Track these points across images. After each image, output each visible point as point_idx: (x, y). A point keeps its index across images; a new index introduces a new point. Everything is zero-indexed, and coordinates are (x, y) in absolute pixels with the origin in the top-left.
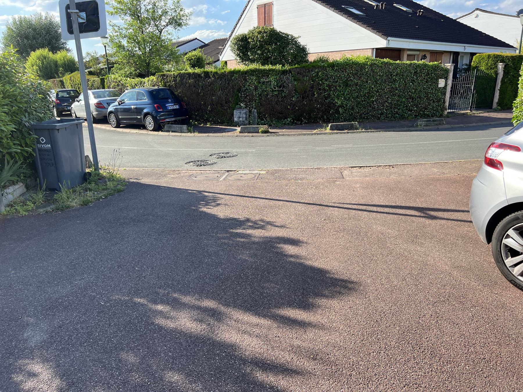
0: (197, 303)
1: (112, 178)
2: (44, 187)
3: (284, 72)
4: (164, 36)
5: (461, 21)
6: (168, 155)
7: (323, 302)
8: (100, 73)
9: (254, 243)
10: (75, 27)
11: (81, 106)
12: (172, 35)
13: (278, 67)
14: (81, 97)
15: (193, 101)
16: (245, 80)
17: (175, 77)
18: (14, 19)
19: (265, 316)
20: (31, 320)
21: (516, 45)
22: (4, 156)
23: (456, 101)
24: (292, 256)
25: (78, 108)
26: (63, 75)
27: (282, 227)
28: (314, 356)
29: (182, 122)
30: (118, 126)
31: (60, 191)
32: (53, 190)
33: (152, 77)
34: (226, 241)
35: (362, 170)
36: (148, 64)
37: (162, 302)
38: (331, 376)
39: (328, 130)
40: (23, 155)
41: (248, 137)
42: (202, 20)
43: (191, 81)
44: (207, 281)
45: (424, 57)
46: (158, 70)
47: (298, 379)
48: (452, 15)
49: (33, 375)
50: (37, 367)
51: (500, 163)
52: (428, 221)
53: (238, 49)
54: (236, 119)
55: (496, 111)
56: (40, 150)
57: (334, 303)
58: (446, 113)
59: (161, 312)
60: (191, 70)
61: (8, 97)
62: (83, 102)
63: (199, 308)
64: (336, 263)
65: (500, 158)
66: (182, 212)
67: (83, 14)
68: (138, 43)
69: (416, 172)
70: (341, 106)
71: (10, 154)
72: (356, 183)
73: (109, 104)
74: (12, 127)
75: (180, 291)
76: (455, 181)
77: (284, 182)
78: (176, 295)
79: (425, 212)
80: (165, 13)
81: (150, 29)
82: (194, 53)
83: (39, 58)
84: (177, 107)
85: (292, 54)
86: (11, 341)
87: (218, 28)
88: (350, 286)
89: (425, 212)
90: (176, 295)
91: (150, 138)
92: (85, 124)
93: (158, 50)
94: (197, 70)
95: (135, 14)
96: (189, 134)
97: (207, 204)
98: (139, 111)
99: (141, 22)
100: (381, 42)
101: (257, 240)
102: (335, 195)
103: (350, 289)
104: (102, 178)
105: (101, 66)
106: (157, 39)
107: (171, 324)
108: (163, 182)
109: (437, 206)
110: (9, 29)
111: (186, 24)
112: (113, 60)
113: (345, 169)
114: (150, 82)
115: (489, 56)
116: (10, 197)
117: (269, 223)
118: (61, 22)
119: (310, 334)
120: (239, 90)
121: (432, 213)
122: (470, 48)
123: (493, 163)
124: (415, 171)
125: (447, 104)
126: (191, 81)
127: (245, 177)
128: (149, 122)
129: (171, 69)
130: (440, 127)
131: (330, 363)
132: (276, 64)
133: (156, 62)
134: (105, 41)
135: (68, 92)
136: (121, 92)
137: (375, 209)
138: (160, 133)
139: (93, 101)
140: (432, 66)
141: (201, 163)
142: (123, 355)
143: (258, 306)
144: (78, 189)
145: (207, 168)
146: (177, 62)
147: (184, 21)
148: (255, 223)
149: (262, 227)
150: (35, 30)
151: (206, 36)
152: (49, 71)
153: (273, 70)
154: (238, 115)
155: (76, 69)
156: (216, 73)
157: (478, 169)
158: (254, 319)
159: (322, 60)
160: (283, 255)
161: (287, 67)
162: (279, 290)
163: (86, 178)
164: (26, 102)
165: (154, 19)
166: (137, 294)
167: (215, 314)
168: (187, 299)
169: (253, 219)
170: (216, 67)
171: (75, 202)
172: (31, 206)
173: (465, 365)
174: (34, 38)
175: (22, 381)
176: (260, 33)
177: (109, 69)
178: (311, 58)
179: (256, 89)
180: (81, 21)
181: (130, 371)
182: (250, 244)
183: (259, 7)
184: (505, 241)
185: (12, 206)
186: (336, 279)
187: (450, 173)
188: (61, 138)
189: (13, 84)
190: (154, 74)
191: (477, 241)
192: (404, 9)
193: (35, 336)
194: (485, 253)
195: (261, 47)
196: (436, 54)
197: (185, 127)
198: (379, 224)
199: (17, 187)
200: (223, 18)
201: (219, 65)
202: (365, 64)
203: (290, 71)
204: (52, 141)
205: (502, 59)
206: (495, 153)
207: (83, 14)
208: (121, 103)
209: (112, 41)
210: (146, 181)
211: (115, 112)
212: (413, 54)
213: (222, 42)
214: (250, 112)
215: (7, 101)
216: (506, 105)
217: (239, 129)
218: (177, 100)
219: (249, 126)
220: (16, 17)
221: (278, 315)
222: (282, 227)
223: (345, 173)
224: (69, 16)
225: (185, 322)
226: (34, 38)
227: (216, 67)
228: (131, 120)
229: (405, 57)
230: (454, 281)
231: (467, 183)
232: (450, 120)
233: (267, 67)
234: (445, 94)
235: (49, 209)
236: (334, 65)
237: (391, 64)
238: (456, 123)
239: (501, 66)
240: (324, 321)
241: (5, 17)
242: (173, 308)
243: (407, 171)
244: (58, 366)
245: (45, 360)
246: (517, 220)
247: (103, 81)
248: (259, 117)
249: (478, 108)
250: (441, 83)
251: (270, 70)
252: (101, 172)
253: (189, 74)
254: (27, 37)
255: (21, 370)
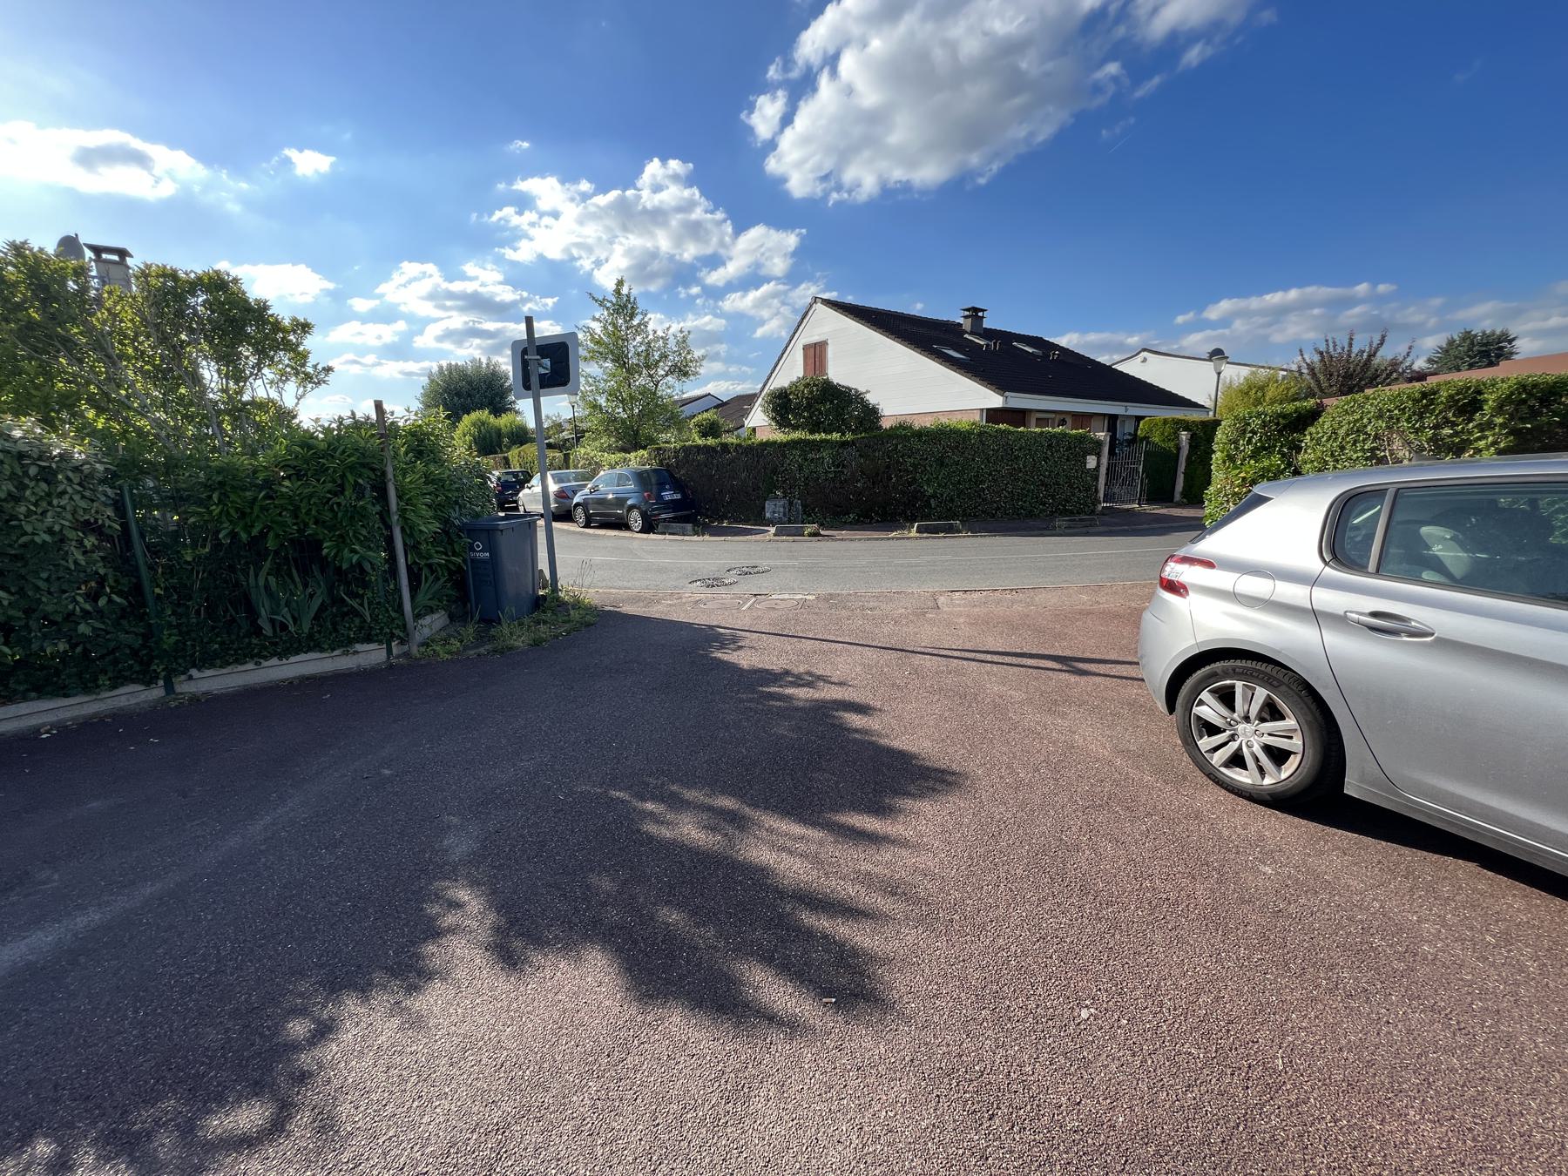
0: (708, 801)
1: (577, 604)
2: (477, 617)
3: (844, 444)
4: (663, 390)
5: (1119, 367)
6: (661, 570)
7: (908, 803)
8: (561, 445)
9: (797, 709)
10: (535, 380)
11: (533, 495)
12: (674, 389)
13: (835, 436)
14: (536, 481)
15: (703, 486)
16: (784, 456)
17: (676, 451)
18: (441, 368)
19: (814, 825)
20: (455, 820)
21: (1208, 404)
22: (420, 569)
23: (1116, 490)
24: (857, 731)
25: (530, 498)
26: (509, 449)
27: (841, 684)
28: (892, 889)
29: (685, 520)
30: (587, 526)
31: (499, 623)
32: (489, 621)
33: (641, 452)
34: (753, 705)
35: (967, 596)
36: (636, 433)
37: (654, 798)
38: (920, 920)
39: (914, 533)
40: (448, 569)
41: (787, 543)
42: (717, 366)
43: (701, 457)
44: (723, 766)
45: (1063, 423)
46: (652, 441)
47: (868, 925)
48: (1104, 359)
49: (457, 905)
50: (463, 895)
51: (1184, 587)
52: (1073, 679)
53: (774, 410)
54: (768, 515)
55: (1179, 505)
56: (472, 561)
57: (925, 806)
58: (1099, 508)
59: (651, 813)
60: (700, 442)
61: (433, 482)
62: (538, 489)
63: (710, 809)
64: (927, 744)
65: (1184, 579)
66: (683, 658)
67: (547, 362)
68: (622, 401)
69: (1054, 601)
70: (934, 496)
71: (430, 566)
72: (1268, 856)
73: (575, 493)
74: (436, 526)
75: (680, 781)
76: (1117, 616)
77: (844, 613)
78: (674, 788)
79: (1069, 663)
80: (664, 356)
81: (641, 381)
82: (705, 415)
83: (474, 424)
84: (678, 496)
85: (857, 417)
86: (424, 851)
87: (742, 378)
88: (950, 779)
89: (1069, 663)
90: (674, 788)
91: (635, 544)
92: (541, 522)
93: (651, 412)
94: (710, 441)
95: (620, 359)
96: (695, 538)
97: (722, 646)
98: (620, 502)
99: (628, 371)
100: (995, 400)
101: (801, 704)
102: (927, 635)
103: (950, 784)
104: (562, 604)
105: (565, 435)
106: (650, 395)
107: (666, 833)
108: (656, 611)
109: (1088, 655)
110: (432, 381)
111: (695, 374)
112: (584, 426)
113: (942, 593)
114: (638, 460)
115: (1165, 422)
116: (426, 631)
117: (820, 678)
118: (328, 278)
119: (887, 854)
120: (774, 471)
121: (1081, 665)
122: (1135, 410)
123: (1174, 587)
124: (1052, 599)
125: (1101, 495)
126: (701, 457)
127: (782, 605)
128: (636, 519)
129: (670, 439)
130: (1092, 530)
131: (917, 901)
132: (831, 432)
133: (647, 430)
134: (573, 398)
135: (515, 475)
136: (594, 473)
137: (989, 657)
138: (652, 536)
139: (553, 487)
140: (1075, 436)
141: (714, 582)
142: (593, 879)
143: (804, 808)
144: (526, 621)
145: (722, 590)
146: (680, 430)
147: (692, 367)
148: (798, 677)
149: (810, 685)
150: (470, 383)
151: (724, 389)
152: (488, 443)
153: (827, 441)
154: (771, 508)
155: (532, 440)
156: (739, 445)
157: (1150, 597)
158: (798, 829)
159: (902, 427)
160: (844, 729)
161: (849, 437)
162: (837, 783)
163: (538, 603)
164: (457, 490)
165: (648, 367)
166: (614, 784)
167: (733, 818)
168: (690, 795)
169: (796, 671)
170: (738, 437)
171: (520, 641)
172: (456, 644)
173: (1137, 908)
174: (469, 395)
175: (438, 914)
176: (807, 385)
177: (578, 439)
178: (886, 424)
179: (800, 468)
180: (542, 371)
181: (604, 904)
182: (791, 710)
183: (806, 348)
184: (1197, 710)
185: (427, 645)
186: (928, 768)
187: (1108, 602)
188: (504, 542)
189: (438, 462)
190: (644, 448)
191: (1153, 709)
192: (1030, 350)
193: (459, 845)
194: (1166, 729)
195: (809, 407)
196: (1082, 419)
197: (689, 526)
198: (995, 682)
199: (436, 616)
200: (750, 364)
201: (744, 433)
202: (970, 433)
203: (853, 443)
204: (491, 547)
205: (1187, 426)
206: (1174, 571)
207: (547, 362)
208: (595, 490)
209: (583, 398)
210: (628, 609)
211: (584, 505)
212: (1044, 418)
213: (749, 399)
214: (791, 503)
215: (431, 488)
216: (1194, 497)
217: (773, 530)
218: (678, 486)
219: (789, 526)
220: (444, 364)
221: (835, 824)
222: (841, 684)
223: (942, 600)
224: (525, 364)
225: (690, 831)
226: (469, 395)
227: (738, 437)
228: (607, 518)
229: (1033, 421)
230: (1117, 775)
231: (1134, 618)
232: (1106, 518)
233: (817, 437)
234: (1097, 479)
235: (482, 650)
236: (921, 434)
237: (1010, 433)
238: (1116, 524)
239: (1184, 436)
240: (909, 834)
241: (426, 364)
242: (671, 807)
243: (1040, 598)
244: (494, 892)
245: (474, 883)
246: (1214, 676)
247: (567, 457)
248: (804, 512)
249: (1150, 501)
250: (1091, 462)
251: (822, 441)
252: (561, 594)
253: (698, 447)
254: (459, 394)
255: (437, 897)
